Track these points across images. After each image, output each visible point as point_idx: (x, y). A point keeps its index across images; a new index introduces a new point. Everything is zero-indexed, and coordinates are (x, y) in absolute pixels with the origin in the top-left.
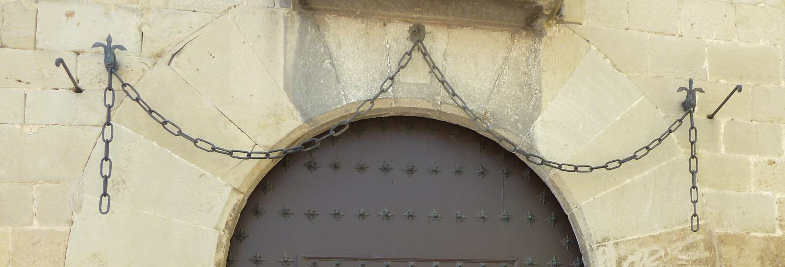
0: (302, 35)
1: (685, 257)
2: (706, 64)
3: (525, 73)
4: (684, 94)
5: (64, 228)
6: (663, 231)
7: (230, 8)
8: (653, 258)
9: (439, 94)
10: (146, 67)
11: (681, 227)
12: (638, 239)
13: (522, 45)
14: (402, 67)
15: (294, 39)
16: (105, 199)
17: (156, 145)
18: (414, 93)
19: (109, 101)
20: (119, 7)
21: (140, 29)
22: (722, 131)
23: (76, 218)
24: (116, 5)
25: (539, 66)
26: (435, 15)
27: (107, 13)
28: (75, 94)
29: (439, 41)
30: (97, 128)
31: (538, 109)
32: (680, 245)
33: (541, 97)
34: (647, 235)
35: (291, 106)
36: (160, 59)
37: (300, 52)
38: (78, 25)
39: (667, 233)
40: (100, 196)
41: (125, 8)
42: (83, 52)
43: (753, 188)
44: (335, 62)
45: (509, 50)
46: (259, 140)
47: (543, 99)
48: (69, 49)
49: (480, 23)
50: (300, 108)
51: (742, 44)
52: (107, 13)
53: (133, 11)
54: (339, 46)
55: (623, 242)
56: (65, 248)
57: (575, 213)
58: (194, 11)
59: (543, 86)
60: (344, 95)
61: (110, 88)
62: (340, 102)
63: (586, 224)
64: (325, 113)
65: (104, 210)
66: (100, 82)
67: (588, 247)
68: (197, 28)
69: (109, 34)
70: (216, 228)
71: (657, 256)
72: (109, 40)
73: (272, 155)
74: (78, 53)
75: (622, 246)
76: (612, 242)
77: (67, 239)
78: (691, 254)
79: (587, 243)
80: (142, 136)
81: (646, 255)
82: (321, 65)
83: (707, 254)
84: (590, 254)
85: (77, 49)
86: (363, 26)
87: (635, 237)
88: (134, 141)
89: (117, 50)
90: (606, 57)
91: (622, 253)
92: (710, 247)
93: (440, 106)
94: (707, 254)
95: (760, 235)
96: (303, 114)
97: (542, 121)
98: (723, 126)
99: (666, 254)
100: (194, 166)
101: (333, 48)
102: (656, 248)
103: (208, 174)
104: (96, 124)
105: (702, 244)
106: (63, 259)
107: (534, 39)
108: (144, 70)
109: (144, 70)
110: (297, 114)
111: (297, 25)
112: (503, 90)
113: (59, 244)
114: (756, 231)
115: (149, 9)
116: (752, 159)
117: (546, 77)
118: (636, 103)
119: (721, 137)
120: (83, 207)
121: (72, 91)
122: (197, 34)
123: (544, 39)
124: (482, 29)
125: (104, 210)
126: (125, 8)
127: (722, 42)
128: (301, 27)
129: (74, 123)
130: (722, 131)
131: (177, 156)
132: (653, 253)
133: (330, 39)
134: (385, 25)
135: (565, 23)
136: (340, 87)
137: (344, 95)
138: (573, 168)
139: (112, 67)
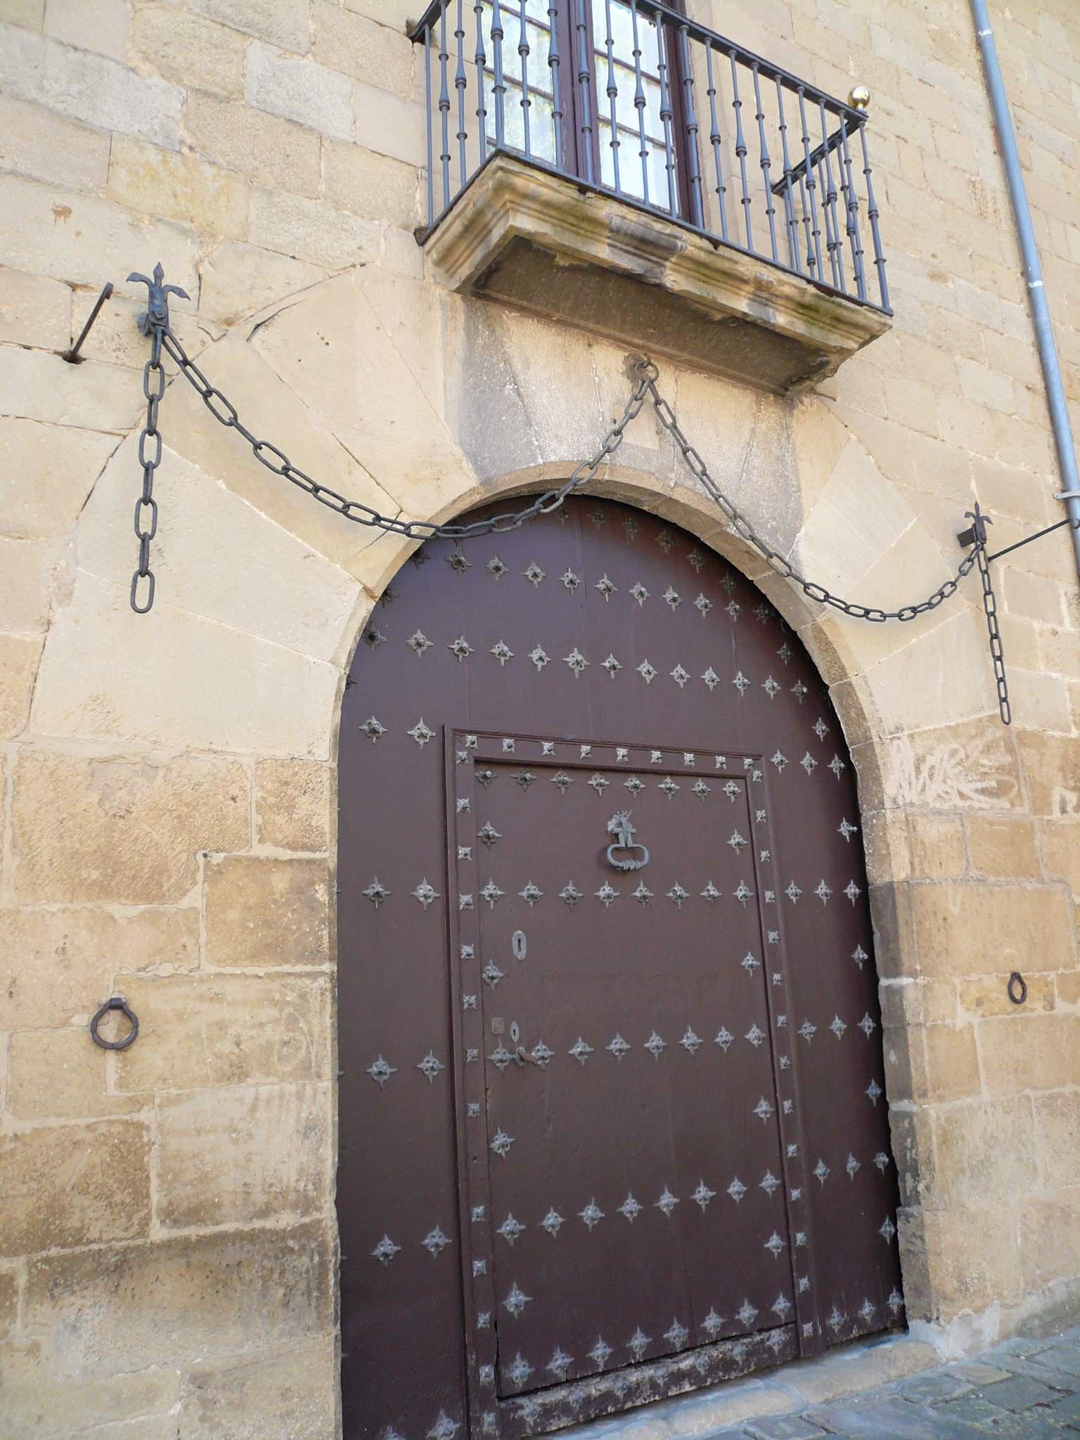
0: (471, 335)
1: (986, 762)
2: (973, 485)
3: (777, 458)
4: (972, 521)
5: (32, 635)
6: (960, 721)
7: (354, 266)
8: (954, 761)
9: (672, 470)
10: (207, 338)
11: (978, 716)
12: (935, 730)
13: (771, 413)
14: (632, 417)
15: (459, 339)
16: (144, 582)
17: (223, 487)
18: (644, 465)
19: (154, 388)
20: (159, 221)
21: (196, 267)
22: (1002, 582)
23: (58, 614)
24: (152, 215)
25: (794, 450)
26: (666, 345)
27: (134, 225)
28: (67, 365)
29: (672, 384)
30: (108, 438)
31: (798, 516)
32: (980, 743)
33: (800, 497)
34: (943, 725)
35: (459, 452)
36: (232, 329)
37: (469, 363)
38: (78, 234)
39: (964, 724)
40: (132, 575)
41: (169, 224)
42: (84, 286)
43: (1042, 667)
44: (522, 390)
45: (756, 418)
46: (408, 504)
47: (804, 501)
48: (58, 276)
49: (719, 373)
50: (473, 457)
51: (1004, 465)
52: (134, 225)
53: (184, 232)
54: (527, 365)
55: (920, 734)
56: (32, 679)
57: (854, 684)
58: (293, 257)
59: (802, 482)
60: (539, 447)
61: (155, 364)
62: (535, 459)
63: (873, 703)
64: (511, 473)
65: (142, 603)
66: (118, 349)
67: (876, 739)
68: (298, 287)
69: (159, 266)
70: (332, 662)
71: (957, 758)
72: (159, 273)
73: (415, 530)
74: (74, 287)
75: (917, 738)
76: (907, 733)
77: (36, 658)
78: (992, 757)
79: (873, 733)
80: (197, 466)
81: (946, 757)
82: (501, 391)
83: (1009, 759)
84: (877, 750)
85: (75, 279)
86: (560, 340)
87: (931, 727)
88: (181, 474)
89: (172, 296)
90: (869, 454)
91: (920, 751)
92: (1011, 750)
93: (672, 489)
94: (1009, 759)
95: (1057, 734)
96: (479, 469)
97: (806, 534)
98: (1002, 574)
99: (967, 757)
100: (293, 536)
101: (518, 366)
102: (955, 746)
103: (319, 554)
104: (108, 429)
105: (1002, 743)
106: (26, 704)
107: (784, 411)
108: (203, 343)
109: (203, 343)
110: (467, 466)
111: (461, 317)
112: (755, 479)
113: (20, 670)
114: (1053, 729)
115: (213, 236)
116: (1037, 625)
117: (804, 467)
118: (910, 525)
119: (1003, 590)
120: (76, 594)
121: (60, 358)
122: (300, 297)
123: (795, 412)
124: (719, 380)
125: (142, 603)
126: (169, 224)
127: (985, 459)
128: (466, 322)
129: (62, 421)
130: (1002, 582)
131: (262, 515)
132: (953, 753)
133: (512, 350)
134: (590, 345)
135: (816, 393)
136: (532, 433)
137: (539, 447)
138: (862, 612)
139: (155, 327)
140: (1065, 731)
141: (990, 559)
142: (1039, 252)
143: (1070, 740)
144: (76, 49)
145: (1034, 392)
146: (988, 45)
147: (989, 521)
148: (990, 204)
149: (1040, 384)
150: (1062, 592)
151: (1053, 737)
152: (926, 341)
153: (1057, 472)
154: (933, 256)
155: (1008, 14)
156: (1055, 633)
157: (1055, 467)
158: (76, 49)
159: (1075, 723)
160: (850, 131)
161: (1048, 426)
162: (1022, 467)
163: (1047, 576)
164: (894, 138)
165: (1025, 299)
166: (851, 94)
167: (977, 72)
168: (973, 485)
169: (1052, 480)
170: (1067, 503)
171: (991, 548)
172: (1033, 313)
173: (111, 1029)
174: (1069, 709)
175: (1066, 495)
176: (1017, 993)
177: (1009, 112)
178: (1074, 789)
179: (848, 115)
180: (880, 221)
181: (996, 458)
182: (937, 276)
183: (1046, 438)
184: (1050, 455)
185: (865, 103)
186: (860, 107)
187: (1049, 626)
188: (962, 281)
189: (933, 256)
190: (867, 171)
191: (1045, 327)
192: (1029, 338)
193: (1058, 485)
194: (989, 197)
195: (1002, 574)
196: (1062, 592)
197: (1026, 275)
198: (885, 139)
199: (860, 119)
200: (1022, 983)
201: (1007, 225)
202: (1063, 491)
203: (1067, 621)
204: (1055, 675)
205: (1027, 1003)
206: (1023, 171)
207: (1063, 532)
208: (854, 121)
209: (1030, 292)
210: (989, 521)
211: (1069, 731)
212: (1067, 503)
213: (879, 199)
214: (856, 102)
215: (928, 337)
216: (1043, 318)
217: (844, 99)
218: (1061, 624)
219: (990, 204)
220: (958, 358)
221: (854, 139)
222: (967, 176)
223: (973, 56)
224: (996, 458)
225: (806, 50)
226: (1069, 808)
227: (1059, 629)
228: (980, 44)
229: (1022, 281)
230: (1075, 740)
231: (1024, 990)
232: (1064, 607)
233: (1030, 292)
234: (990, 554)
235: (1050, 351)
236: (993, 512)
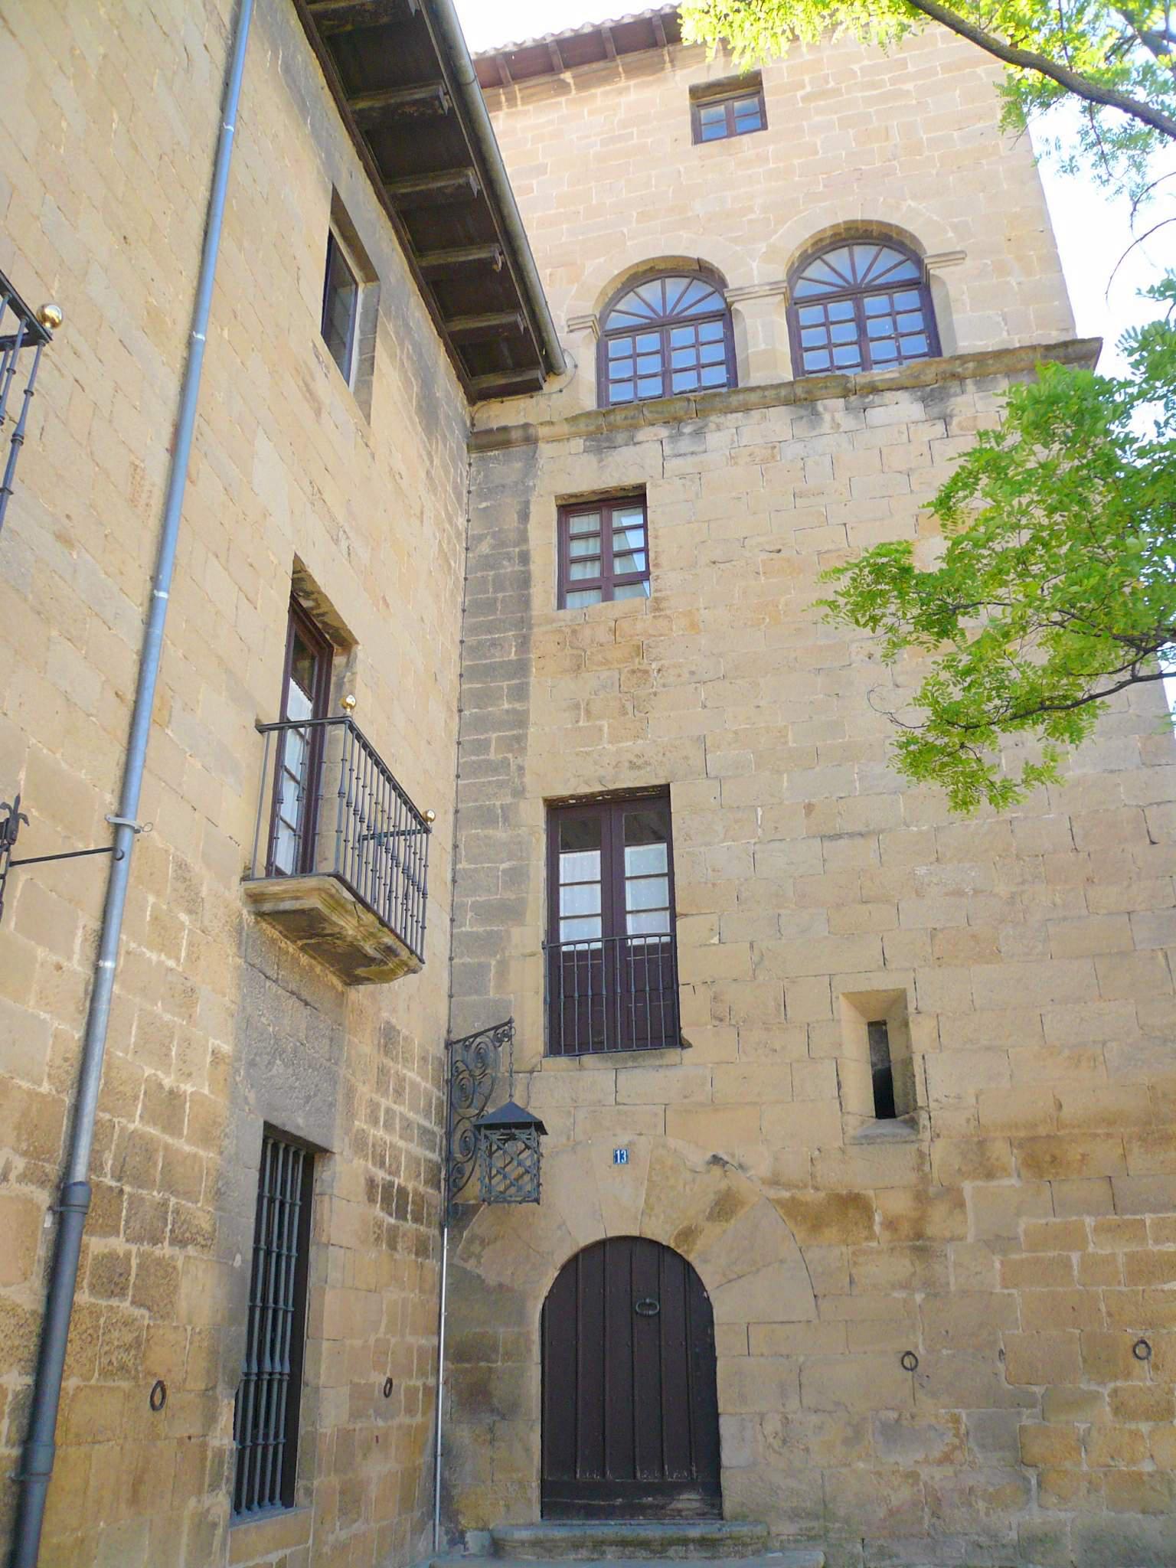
2: (22, 775)
4: (6, 814)
22: (18, 894)
51: (64, 766)
95: (25, 1085)
98: (20, 885)
114: (23, 1079)
116: (41, 952)
130: (18, 894)
140: (34, 1082)
141: (12, 864)
142: (175, 565)
143: (37, 1094)
144: (861, 835)
145: (122, 700)
146: (198, 348)
147: (26, 822)
148: (144, 495)
149: (130, 697)
150: (81, 924)
151: (20, 1087)
152: (26, 600)
153: (117, 793)
154: (68, 516)
155: (226, 334)
156: (59, 967)
157: (117, 787)
158: (861, 835)
159: (49, 1076)
160: (26, 343)
161: (125, 742)
162: (82, 775)
163: (70, 901)
164: (71, 379)
165: (146, 604)
166: (43, 307)
167: (178, 366)
168: (22, 775)
169: (110, 799)
170: (117, 828)
171: (18, 851)
172: (149, 622)
173: (1141, 1350)
174: (48, 1058)
175: (119, 820)
176: (157, 1400)
177: (195, 422)
178: (25, 1154)
179: (30, 325)
180: (23, 452)
181: (58, 756)
182: (64, 539)
183: (118, 753)
184: (116, 773)
185: (54, 325)
186: (48, 325)
187: (54, 958)
188: (88, 557)
189: (68, 516)
190: (28, 392)
191: (155, 640)
192: (136, 645)
193: (115, 807)
194: (146, 488)
195: (20, 885)
196: (81, 924)
197: (155, 581)
198: (62, 375)
199: (42, 337)
200: (164, 1391)
201: (153, 523)
202: (117, 816)
203: (76, 957)
204: (43, 1015)
205: (163, 1411)
206: (188, 483)
207: (103, 859)
208: (35, 334)
209: (153, 599)
210: (26, 822)
211: (40, 1085)
212: (117, 828)
213: (31, 430)
214: (45, 318)
215: (30, 597)
216: (157, 631)
217: (34, 307)
218: (69, 959)
219: (144, 495)
220: (54, 633)
221: (28, 353)
222: (133, 458)
223: (181, 351)
224: (58, 756)
225: (14, 240)
226: (12, 1176)
227: (65, 964)
228: (190, 343)
229: (149, 585)
230: (43, 1095)
231: (164, 1397)
232: (78, 940)
233: (153, 599)
234: (14, 859)
235: (152, 666)
236: (35, 812)
